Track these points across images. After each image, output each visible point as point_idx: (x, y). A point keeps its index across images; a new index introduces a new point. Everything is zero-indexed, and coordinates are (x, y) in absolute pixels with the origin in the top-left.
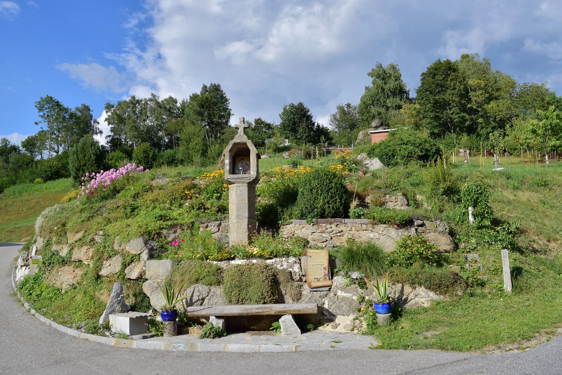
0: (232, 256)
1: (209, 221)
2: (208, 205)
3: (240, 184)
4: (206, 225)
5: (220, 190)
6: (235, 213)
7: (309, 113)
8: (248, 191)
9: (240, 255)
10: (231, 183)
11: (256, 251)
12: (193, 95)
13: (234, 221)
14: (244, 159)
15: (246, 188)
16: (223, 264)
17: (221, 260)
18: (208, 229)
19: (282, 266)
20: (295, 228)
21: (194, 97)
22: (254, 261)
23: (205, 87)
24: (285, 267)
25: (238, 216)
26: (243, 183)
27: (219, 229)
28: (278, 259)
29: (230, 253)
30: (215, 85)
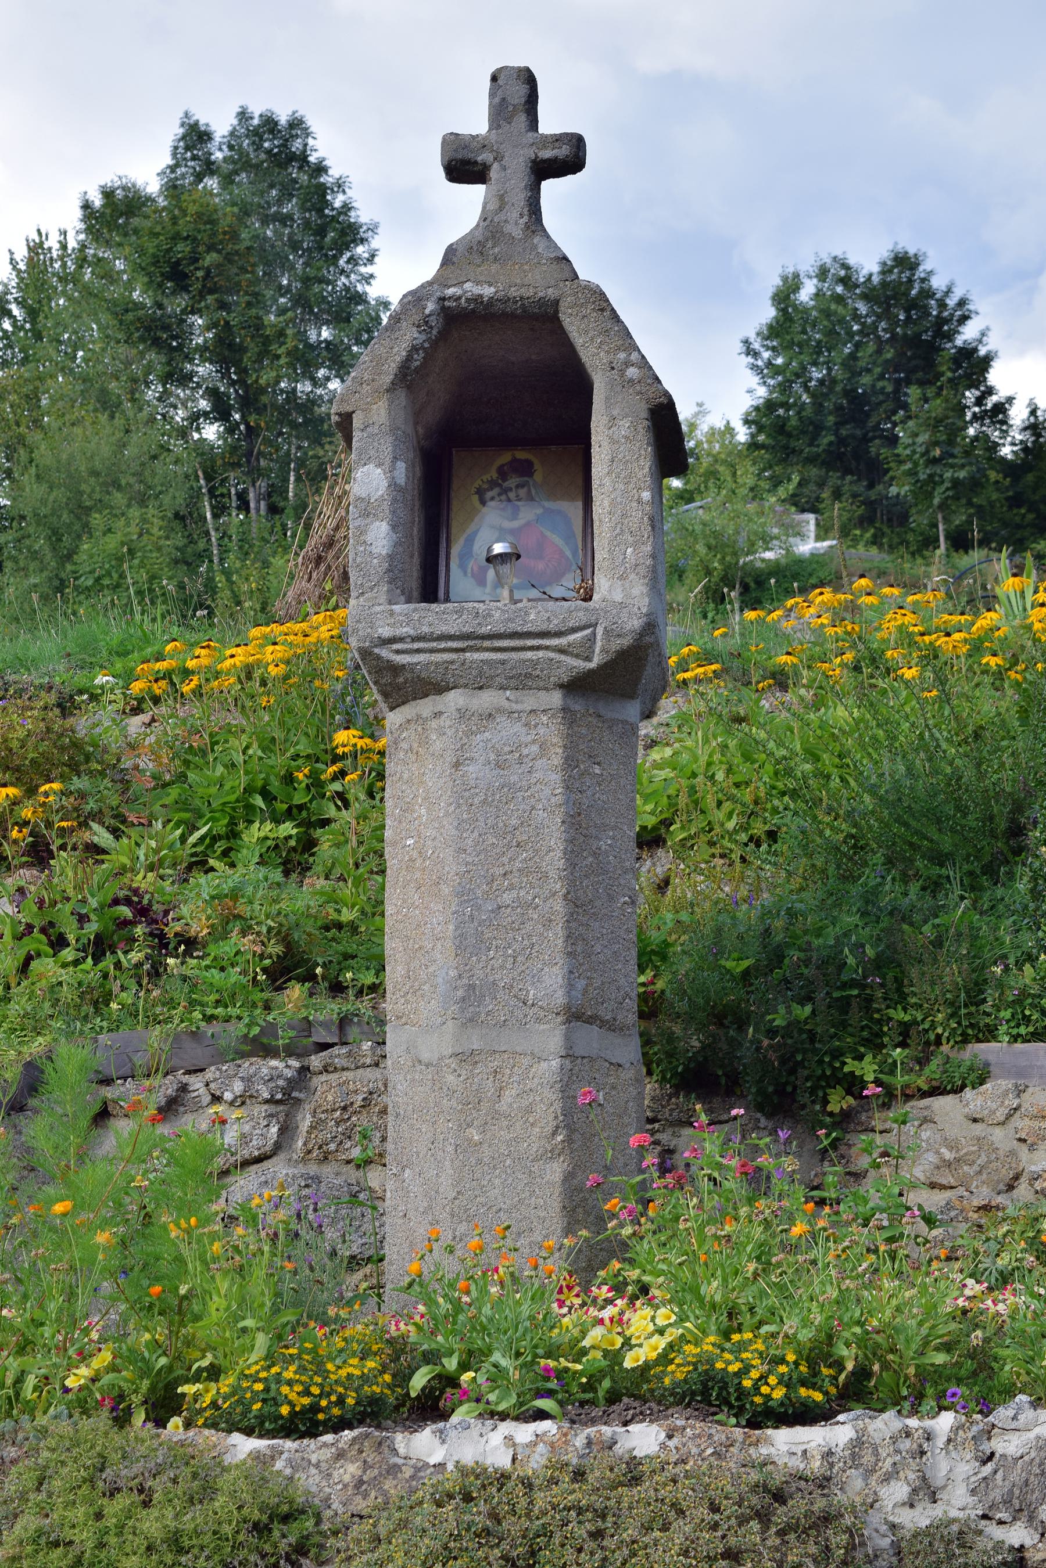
0: (419, 1381)
1: (195, 1053)
2: (193, 915)
3: (488, 699)
4: (168, 1087)
5: (309, 804)
6: (443, 965)
7: (968, 333)
8: (570, 762)
9: (498, 1376)
10: (403, 686)
11: (647, 1333)
12: (108, 194)
13: (437, 1045)
14: (525, 469)
15: (551, 731)
16: (323, 1470)
17: (304, 1425)
18: (194, 1123)
19: (927, 1490)
20: (1022, 1124)
21: (114, 214)
22: (644, 1439)
23: (195, 136)
24: (958, 1503)
25: (471, 1001)
26: (523, 680)
27: (287, 1130)
28: (884, 1425)
29: (400, 1356)
30: (269, 123)
